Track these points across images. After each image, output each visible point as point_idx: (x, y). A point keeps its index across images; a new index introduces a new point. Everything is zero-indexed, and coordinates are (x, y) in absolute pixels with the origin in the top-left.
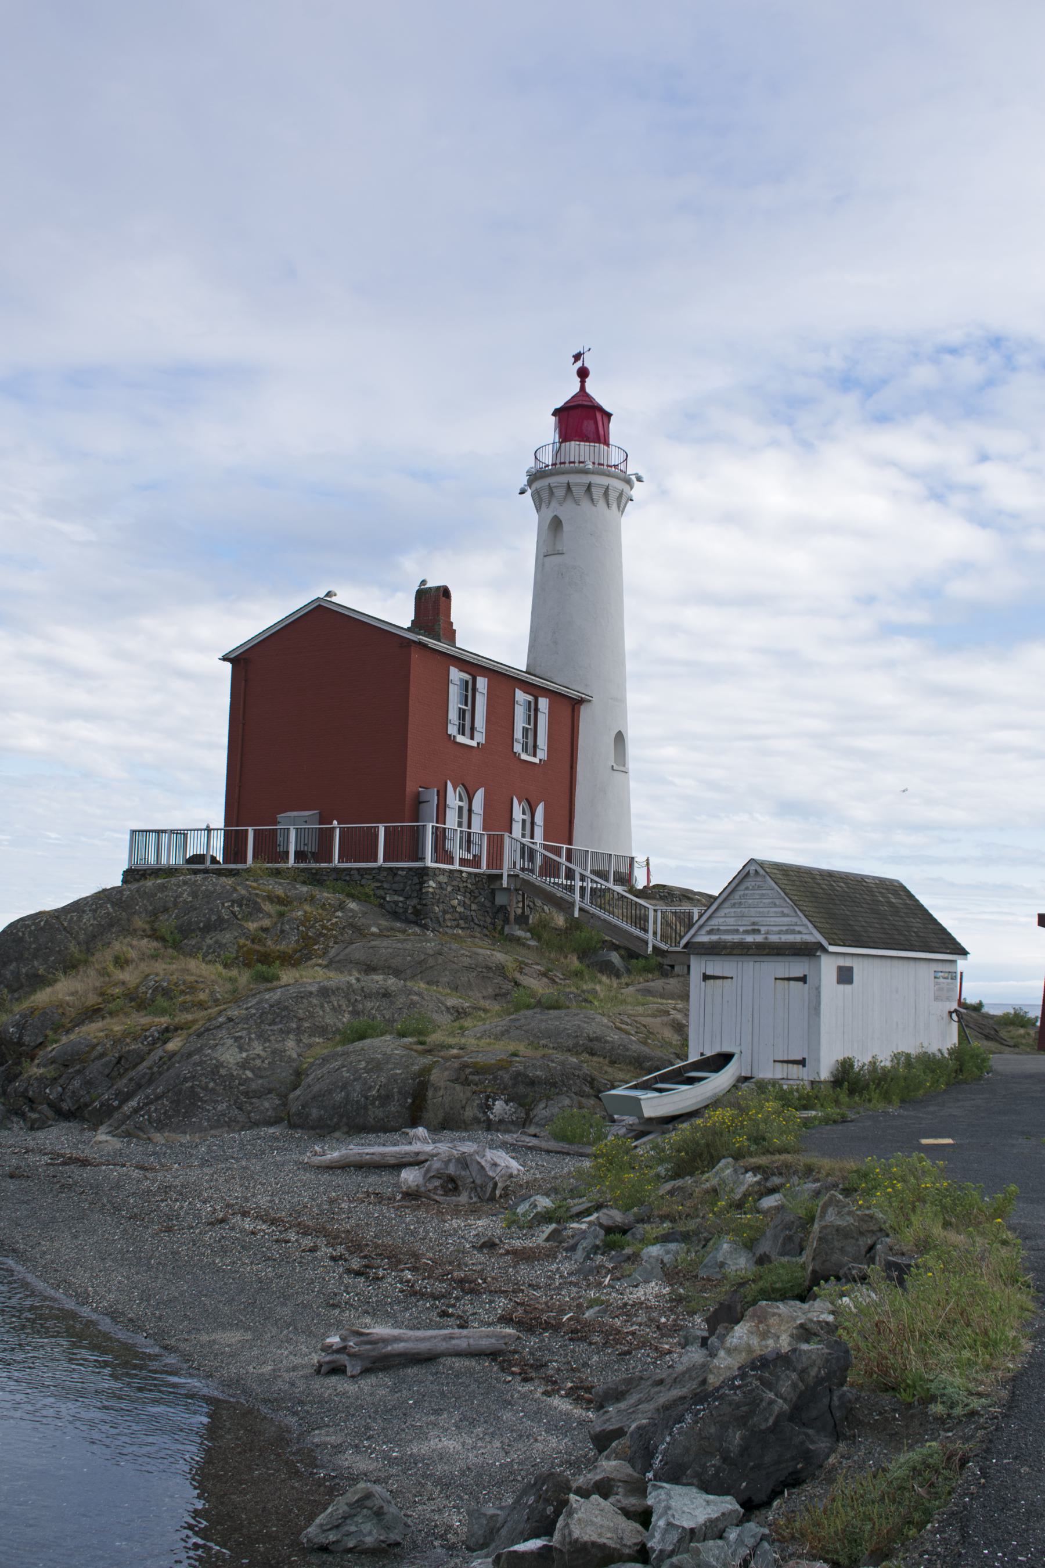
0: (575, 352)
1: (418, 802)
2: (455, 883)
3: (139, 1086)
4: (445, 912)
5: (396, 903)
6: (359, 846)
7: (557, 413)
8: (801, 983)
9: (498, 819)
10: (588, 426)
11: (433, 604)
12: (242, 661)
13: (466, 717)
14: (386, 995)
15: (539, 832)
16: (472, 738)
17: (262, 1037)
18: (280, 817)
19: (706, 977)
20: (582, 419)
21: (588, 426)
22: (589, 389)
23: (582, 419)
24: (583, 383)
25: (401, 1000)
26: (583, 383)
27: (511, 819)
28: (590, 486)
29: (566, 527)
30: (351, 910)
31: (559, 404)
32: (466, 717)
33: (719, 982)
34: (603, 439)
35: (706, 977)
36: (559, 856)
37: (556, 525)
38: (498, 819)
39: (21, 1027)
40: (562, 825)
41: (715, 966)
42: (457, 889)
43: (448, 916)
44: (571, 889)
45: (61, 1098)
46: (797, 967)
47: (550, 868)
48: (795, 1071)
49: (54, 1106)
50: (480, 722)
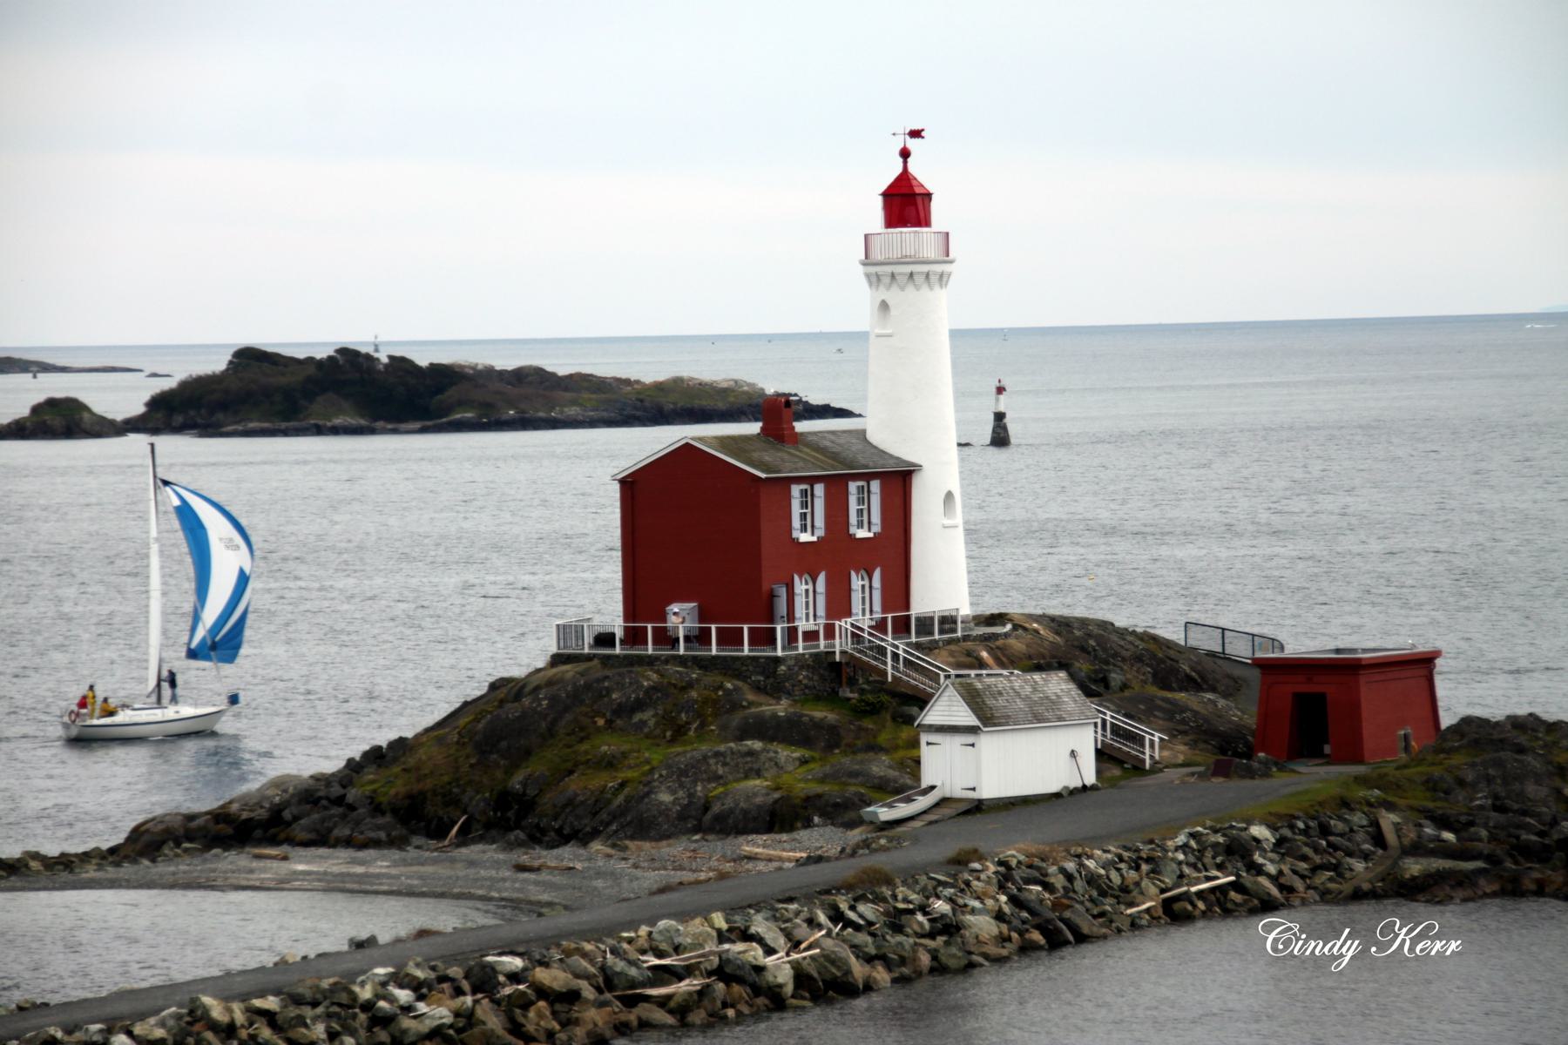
1: (772, 596)
3: (615, 818)
9: (839, 604)
10: (910, 211)
12: (633, 486)
17: (682, 786)
20: (905, 203)
21: (910, 211)
22: (912, 169)
23: (905, 203)
24: (905, 163)
25: (763, 757)
26: (905, 163)
28: (911, 274)
29: (893, 312)
31: (884, 187)
34: (922, 220)
37: (884, 306)
39: (524, 784)
40: (898, 589)
41: (933, 738)
42: (802, 668)
45: (561, 828)
46: (970, 739)
48: (525, 859)
49: (559, 831)
50: (820, 521)
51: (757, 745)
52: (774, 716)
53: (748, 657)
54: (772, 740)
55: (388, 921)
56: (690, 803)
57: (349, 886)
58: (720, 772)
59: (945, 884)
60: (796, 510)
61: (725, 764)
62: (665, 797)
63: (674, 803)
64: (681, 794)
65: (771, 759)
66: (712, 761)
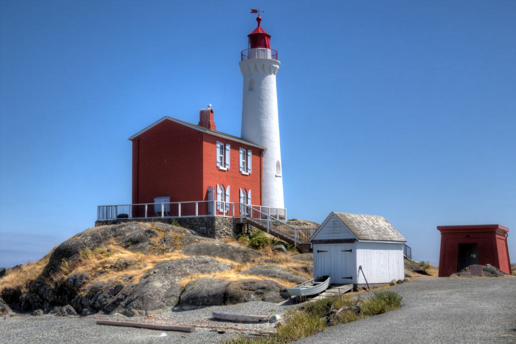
0: (254, 9)
2: (224, 222)
4: (221, 233)
5: (203, 230)
6: (188, 209)
7: (332, 215)
8: (349, 252)
11: (205, 118)
12: (138, 142)
13: (223, 159)
14: (206, 262)
15: (228, 198)
16: (225, 167)
17: (167, 278)
18: (155, 200)
19: (318, 251)
24: (259, 23)
25: (211, 263)
26: (259, 23)
27: (240, 197)
30: (188, 233)
32: (223, 159)
33: (323, 253)
35: (318, 251)
36: (259, 210)
38: (235, 196)
43: (222, 234)
44: (266, 223)
45: (94, 303)
46: (348, 246)
47: (256, 214)
51: (208, 258)
52: (214, 245)
53: (198, 218)
54: (214, 255)
55: (218, 275)
56: (172, 288)
57: (387, 264)
58: (188, 272)
59: (36, 302)
60: (219, 155)
61: (191, 267)
62: (158, 284)
63: (162, 288)
64: (166, 282)
65: (216, 266)
66: (184, 265)
